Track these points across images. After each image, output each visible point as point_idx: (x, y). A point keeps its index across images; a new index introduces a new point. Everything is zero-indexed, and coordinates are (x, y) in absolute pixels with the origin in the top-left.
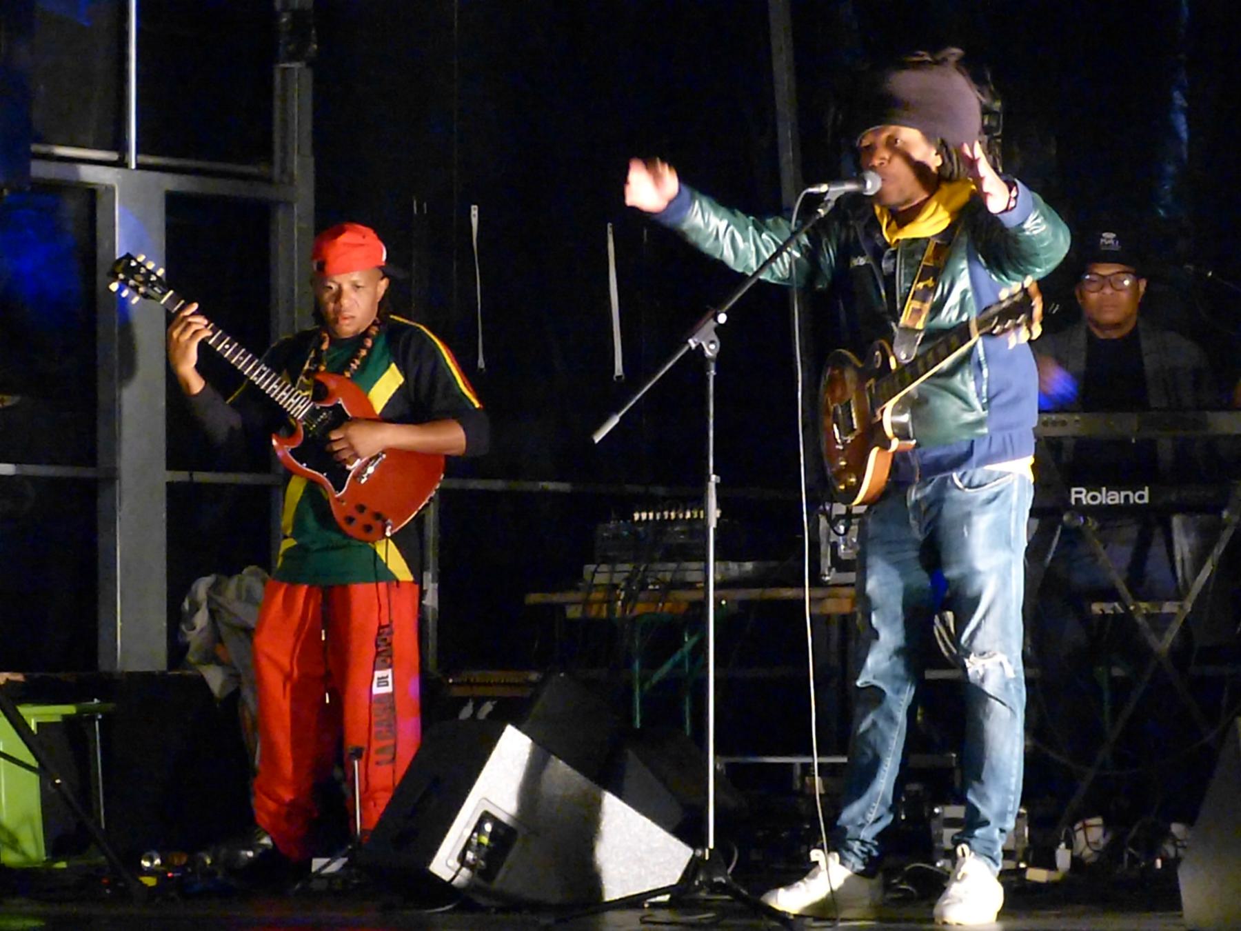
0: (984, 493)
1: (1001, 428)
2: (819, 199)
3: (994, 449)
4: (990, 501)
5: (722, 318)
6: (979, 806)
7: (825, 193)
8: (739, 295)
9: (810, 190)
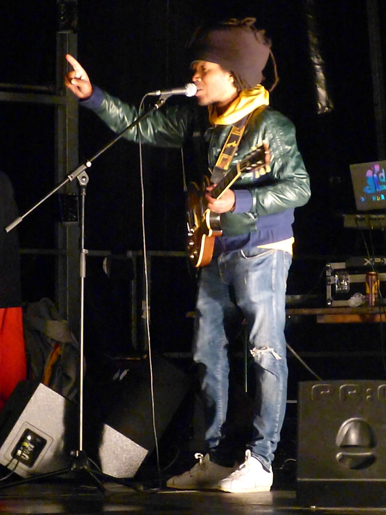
0: (256, 260)
1: (265, 227)
2: (157, 98)
3: (262, 237)
4: (258, 264)
5: (89, 164)
6: (259, 429)
7: (160, 95)
8: (103, 151)
9: (150, 94)
